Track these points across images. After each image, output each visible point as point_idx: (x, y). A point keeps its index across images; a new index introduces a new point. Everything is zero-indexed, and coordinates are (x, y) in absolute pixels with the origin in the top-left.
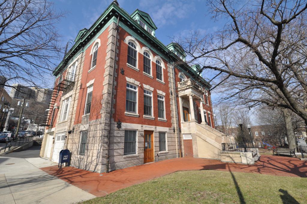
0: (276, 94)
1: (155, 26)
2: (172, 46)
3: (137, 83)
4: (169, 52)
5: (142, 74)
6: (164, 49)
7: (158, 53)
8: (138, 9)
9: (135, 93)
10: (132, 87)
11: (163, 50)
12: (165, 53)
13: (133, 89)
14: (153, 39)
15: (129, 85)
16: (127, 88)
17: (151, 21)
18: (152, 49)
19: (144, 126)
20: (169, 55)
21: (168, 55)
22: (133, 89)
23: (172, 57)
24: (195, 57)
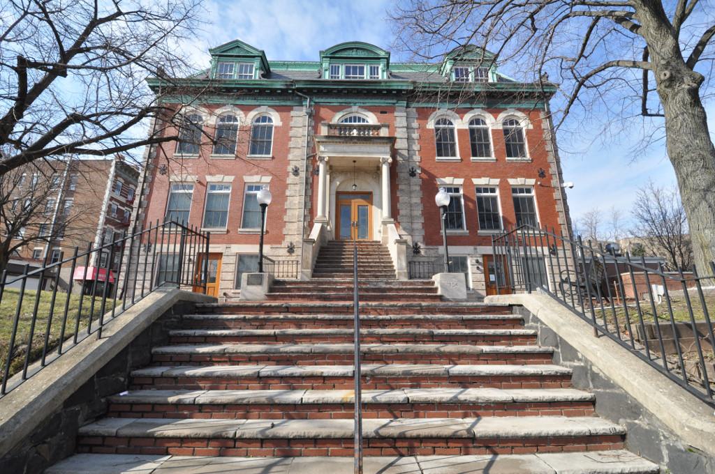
0: (674, 393)
1: (257, 50)
2: (260, 58)
3: (496, 181)
4: (286, 85)
5: (469, 164)
6: (270, 87)
7: (258, 103)
8: (322, 50)
9: (494, 199)
10: (522, 191)
11: (268, 89)
12: (279, 91)
13: (489, 194)
14: (236, 84)
15: (523, 189)
16: (515, 195)
17: (246, 48)
18: (239, 102)
19: (479, 248)
20: (291, 89)
21: (290, 91)
22: (489, 194)
23: (299, 90)
24: (5, 40)
